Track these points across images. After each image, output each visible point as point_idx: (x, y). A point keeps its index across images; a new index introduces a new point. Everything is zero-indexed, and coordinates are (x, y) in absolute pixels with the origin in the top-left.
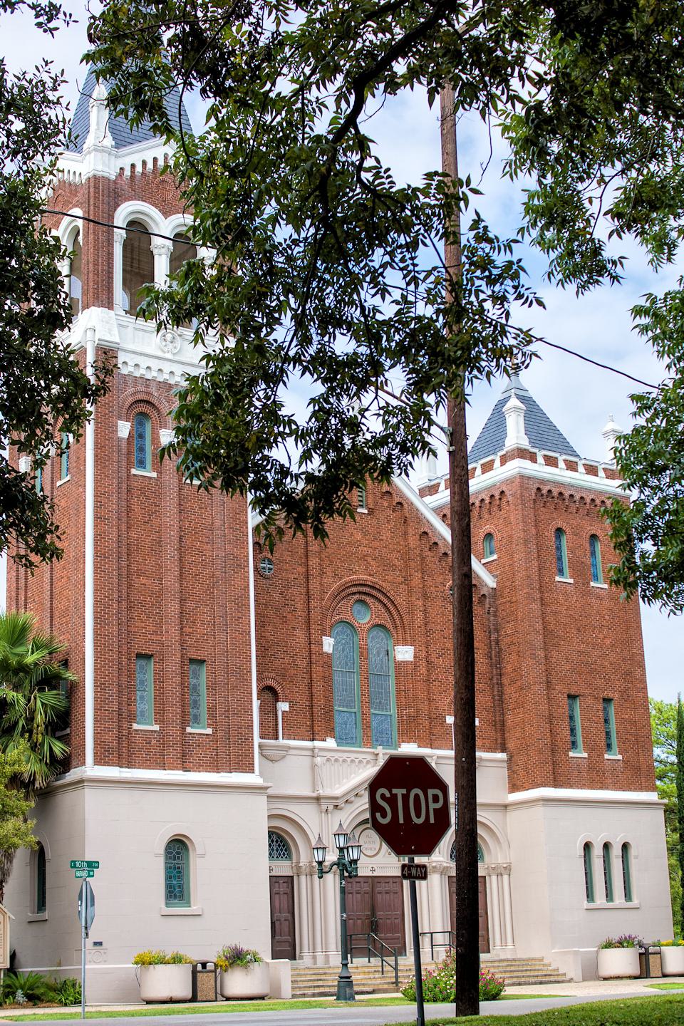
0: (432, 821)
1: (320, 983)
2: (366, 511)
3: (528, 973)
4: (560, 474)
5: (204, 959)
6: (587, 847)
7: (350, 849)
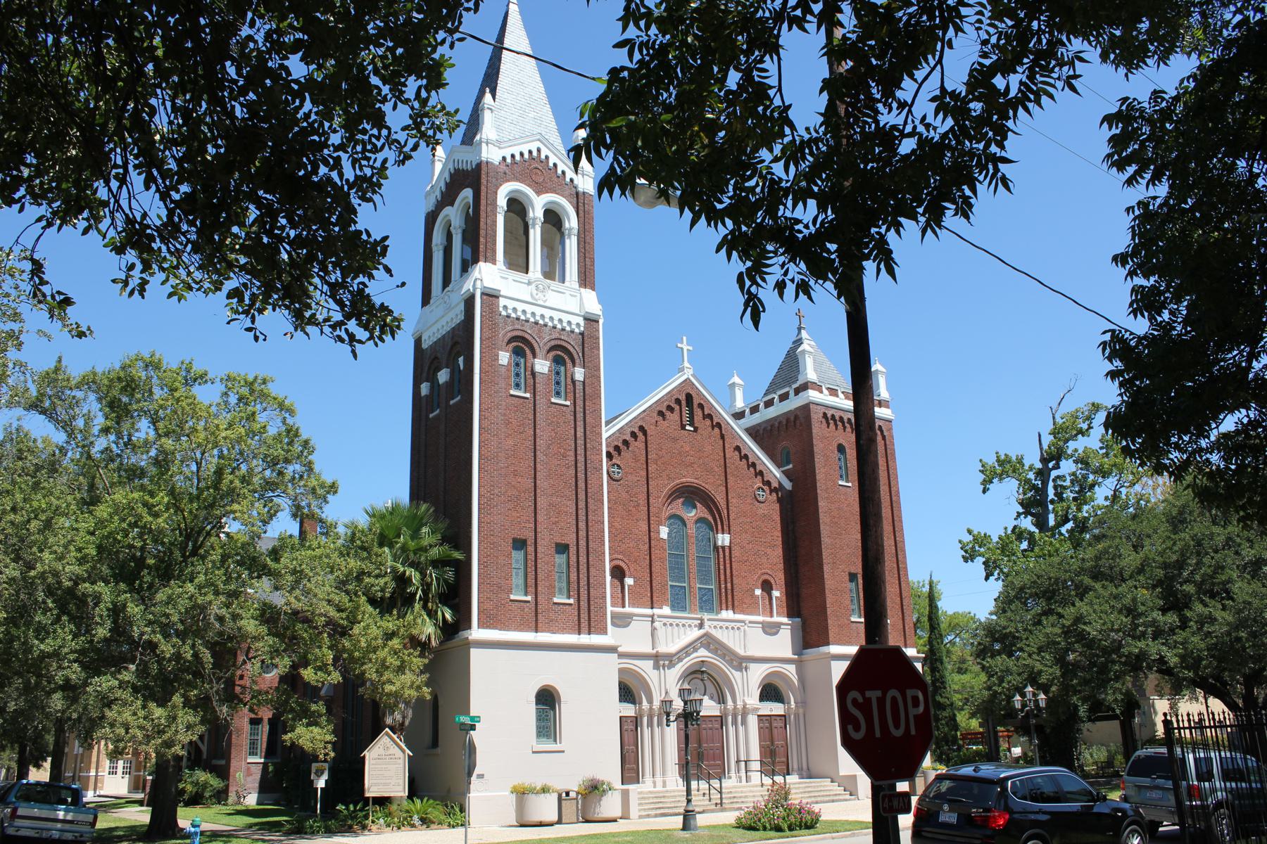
0: (913, 732)
1: (661, 805)
3: (822, 793)
5: (568, 788)
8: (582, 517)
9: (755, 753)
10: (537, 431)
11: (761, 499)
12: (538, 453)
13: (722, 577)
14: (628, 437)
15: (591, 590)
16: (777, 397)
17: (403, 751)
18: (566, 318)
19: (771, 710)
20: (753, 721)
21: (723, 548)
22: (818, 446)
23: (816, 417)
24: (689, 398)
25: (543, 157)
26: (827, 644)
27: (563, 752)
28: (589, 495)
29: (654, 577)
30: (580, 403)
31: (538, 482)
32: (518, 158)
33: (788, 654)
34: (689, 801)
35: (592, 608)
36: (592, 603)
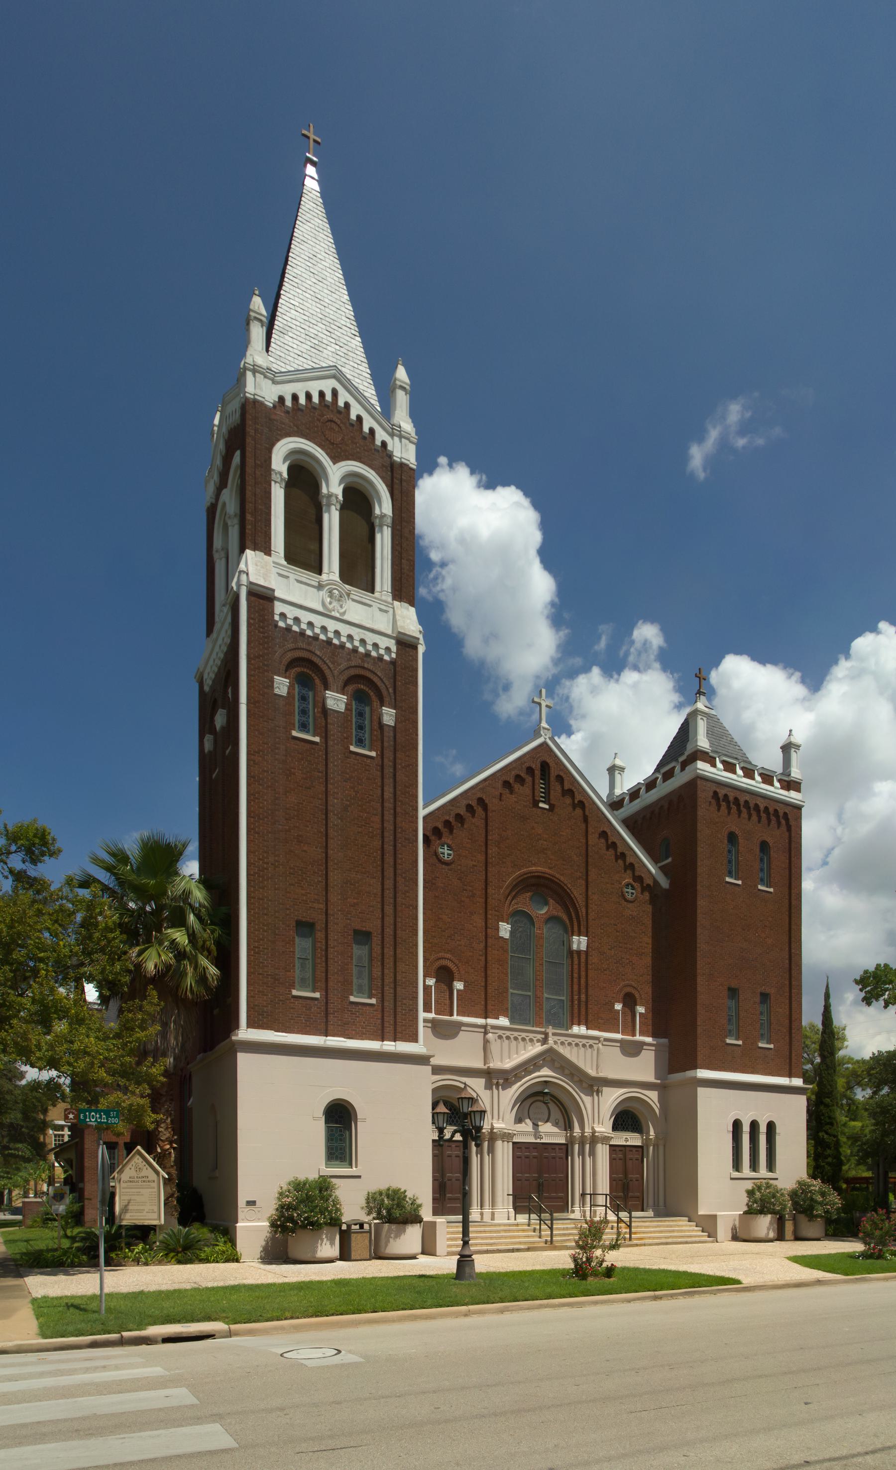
2: (547, 807)
4: (738, 778)
6: (737, 1125)
7: (472, 1114)
8: (389, 899)
9: (604, 1185)
10: (330, 786)
11: (629, 897)
12: (331, 815)
13: (576, 988)
14: (462, 811)
15: (398, 989)
16: (660, 777)
17: (157, 1173)
18: (371, 638)
19: (627, 1140)
20: (603, 1153)
21: (579, 952)
22: (703, 832)
23: (704, 795)
24: (545, 766)
25: (341, 403)
26: (695, 1067)
27: (359, 1177)
28: (399, 872)
29: (489, 981)
30: (389, 754)
31: (330, 852)
32: (302, 400)
33: (649, 1077)
34: (466, 1243)
35: (399, 1009)
36: (399, 1004)
